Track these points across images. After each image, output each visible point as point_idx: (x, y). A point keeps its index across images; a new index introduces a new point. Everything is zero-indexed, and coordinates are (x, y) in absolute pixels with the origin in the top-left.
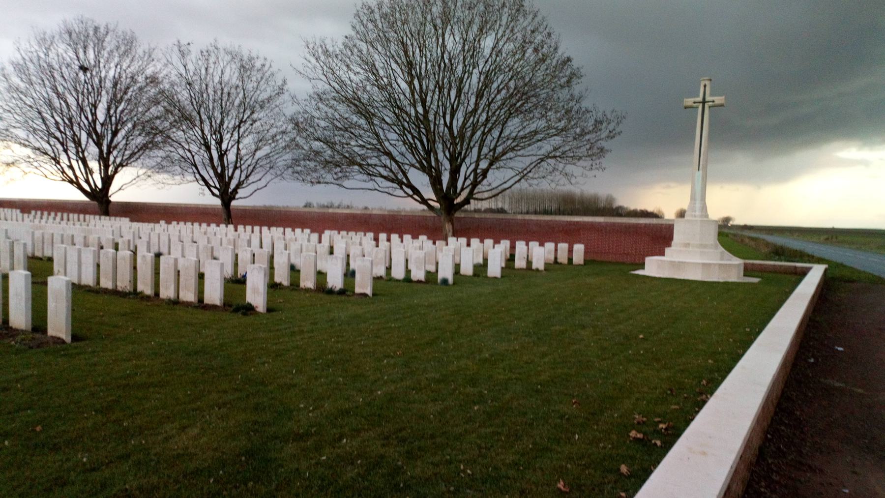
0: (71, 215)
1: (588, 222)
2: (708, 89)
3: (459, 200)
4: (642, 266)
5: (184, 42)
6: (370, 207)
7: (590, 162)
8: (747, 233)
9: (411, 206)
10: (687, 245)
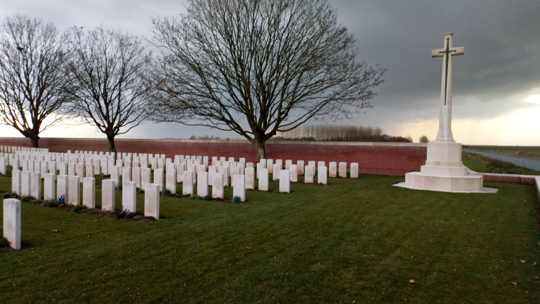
1: (361, 146)
2: (450, 41)
3: (268, 131)
4: (402, 179)
5: (79, 26)
6: (231, 138)
7: (362, 102)
8: (485, 154)
9: (234, 136)
10: (438, 163)
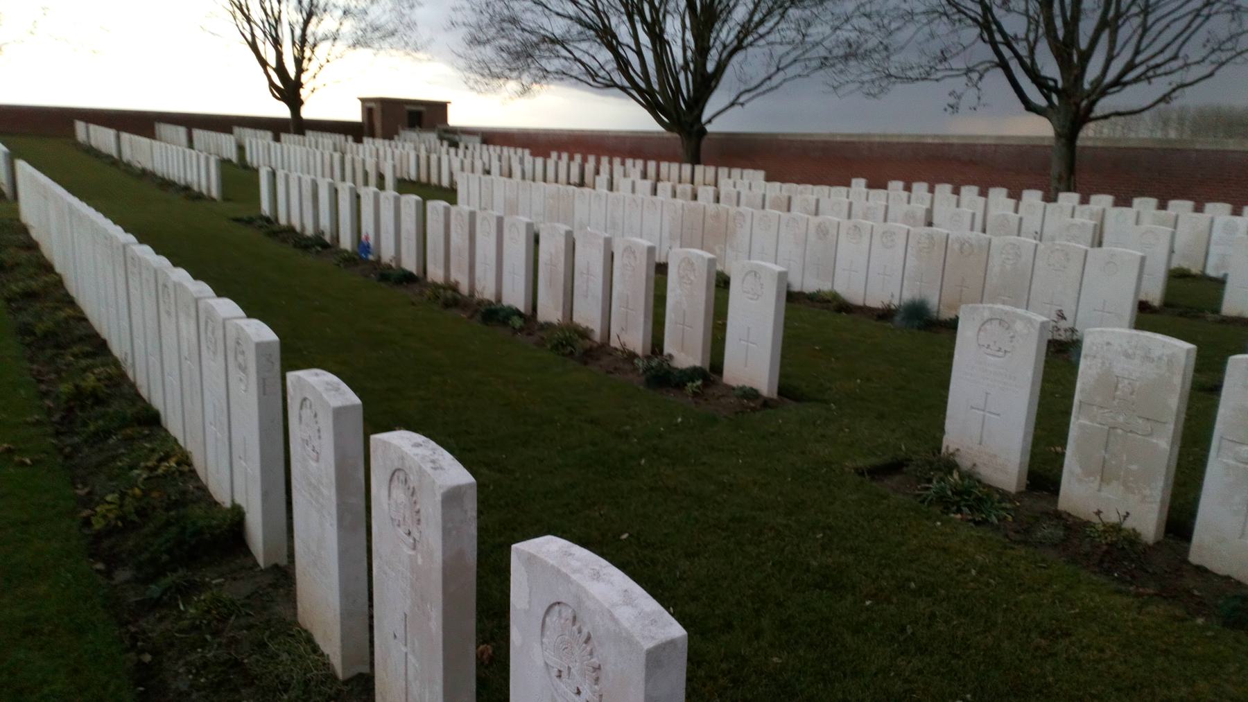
0: (664, 166)
